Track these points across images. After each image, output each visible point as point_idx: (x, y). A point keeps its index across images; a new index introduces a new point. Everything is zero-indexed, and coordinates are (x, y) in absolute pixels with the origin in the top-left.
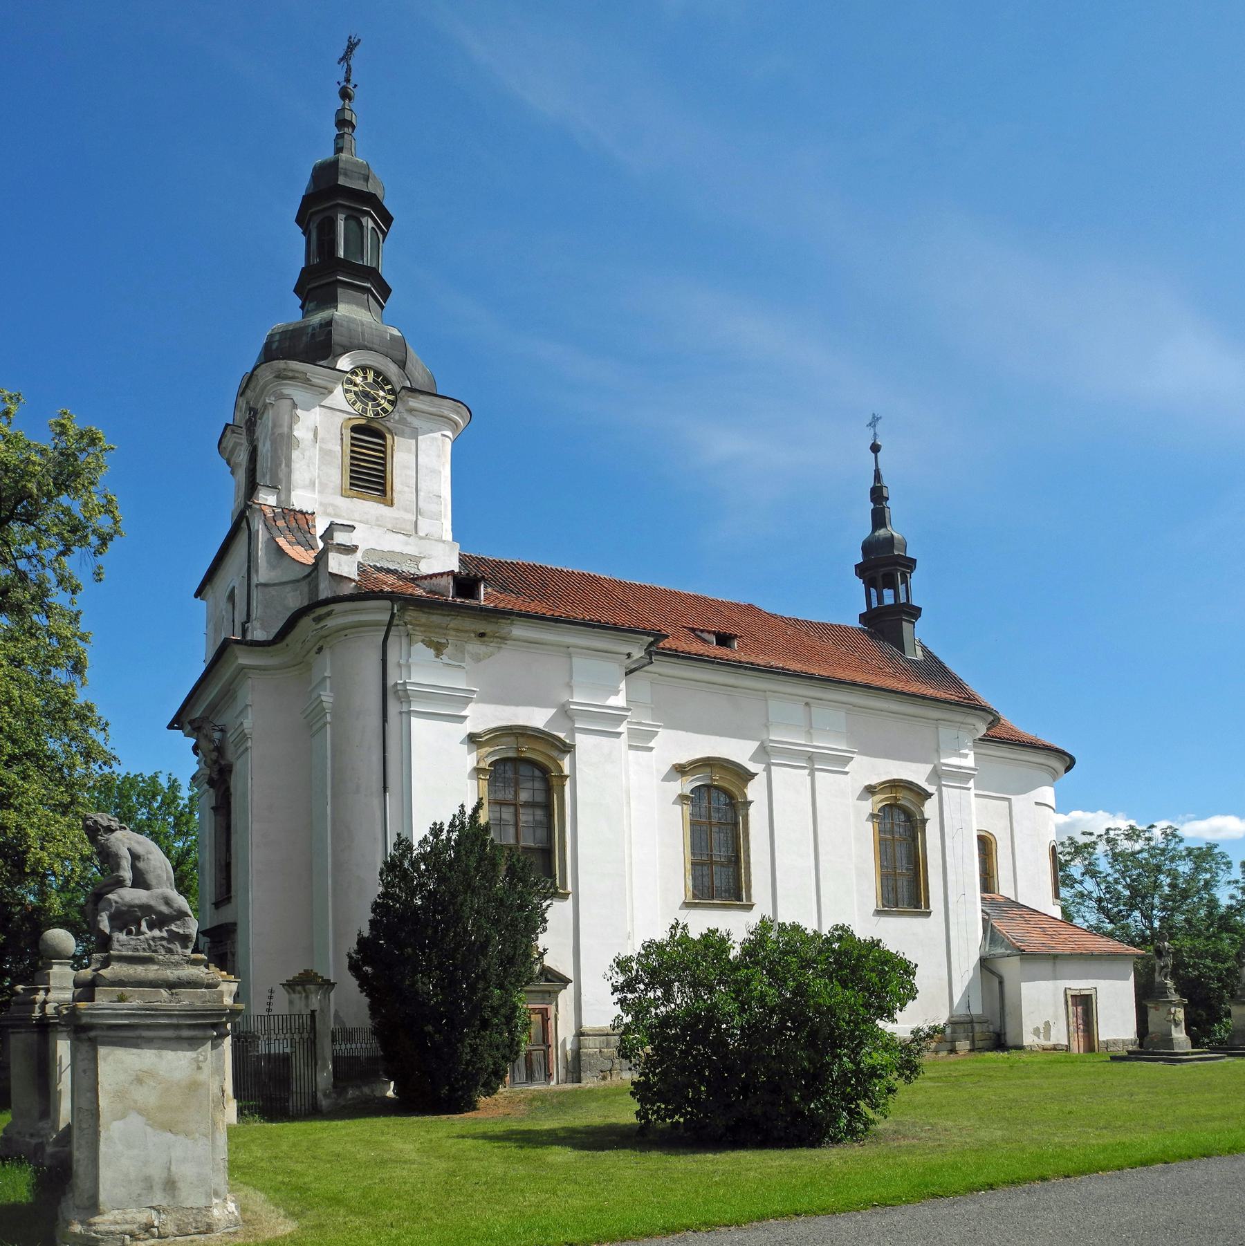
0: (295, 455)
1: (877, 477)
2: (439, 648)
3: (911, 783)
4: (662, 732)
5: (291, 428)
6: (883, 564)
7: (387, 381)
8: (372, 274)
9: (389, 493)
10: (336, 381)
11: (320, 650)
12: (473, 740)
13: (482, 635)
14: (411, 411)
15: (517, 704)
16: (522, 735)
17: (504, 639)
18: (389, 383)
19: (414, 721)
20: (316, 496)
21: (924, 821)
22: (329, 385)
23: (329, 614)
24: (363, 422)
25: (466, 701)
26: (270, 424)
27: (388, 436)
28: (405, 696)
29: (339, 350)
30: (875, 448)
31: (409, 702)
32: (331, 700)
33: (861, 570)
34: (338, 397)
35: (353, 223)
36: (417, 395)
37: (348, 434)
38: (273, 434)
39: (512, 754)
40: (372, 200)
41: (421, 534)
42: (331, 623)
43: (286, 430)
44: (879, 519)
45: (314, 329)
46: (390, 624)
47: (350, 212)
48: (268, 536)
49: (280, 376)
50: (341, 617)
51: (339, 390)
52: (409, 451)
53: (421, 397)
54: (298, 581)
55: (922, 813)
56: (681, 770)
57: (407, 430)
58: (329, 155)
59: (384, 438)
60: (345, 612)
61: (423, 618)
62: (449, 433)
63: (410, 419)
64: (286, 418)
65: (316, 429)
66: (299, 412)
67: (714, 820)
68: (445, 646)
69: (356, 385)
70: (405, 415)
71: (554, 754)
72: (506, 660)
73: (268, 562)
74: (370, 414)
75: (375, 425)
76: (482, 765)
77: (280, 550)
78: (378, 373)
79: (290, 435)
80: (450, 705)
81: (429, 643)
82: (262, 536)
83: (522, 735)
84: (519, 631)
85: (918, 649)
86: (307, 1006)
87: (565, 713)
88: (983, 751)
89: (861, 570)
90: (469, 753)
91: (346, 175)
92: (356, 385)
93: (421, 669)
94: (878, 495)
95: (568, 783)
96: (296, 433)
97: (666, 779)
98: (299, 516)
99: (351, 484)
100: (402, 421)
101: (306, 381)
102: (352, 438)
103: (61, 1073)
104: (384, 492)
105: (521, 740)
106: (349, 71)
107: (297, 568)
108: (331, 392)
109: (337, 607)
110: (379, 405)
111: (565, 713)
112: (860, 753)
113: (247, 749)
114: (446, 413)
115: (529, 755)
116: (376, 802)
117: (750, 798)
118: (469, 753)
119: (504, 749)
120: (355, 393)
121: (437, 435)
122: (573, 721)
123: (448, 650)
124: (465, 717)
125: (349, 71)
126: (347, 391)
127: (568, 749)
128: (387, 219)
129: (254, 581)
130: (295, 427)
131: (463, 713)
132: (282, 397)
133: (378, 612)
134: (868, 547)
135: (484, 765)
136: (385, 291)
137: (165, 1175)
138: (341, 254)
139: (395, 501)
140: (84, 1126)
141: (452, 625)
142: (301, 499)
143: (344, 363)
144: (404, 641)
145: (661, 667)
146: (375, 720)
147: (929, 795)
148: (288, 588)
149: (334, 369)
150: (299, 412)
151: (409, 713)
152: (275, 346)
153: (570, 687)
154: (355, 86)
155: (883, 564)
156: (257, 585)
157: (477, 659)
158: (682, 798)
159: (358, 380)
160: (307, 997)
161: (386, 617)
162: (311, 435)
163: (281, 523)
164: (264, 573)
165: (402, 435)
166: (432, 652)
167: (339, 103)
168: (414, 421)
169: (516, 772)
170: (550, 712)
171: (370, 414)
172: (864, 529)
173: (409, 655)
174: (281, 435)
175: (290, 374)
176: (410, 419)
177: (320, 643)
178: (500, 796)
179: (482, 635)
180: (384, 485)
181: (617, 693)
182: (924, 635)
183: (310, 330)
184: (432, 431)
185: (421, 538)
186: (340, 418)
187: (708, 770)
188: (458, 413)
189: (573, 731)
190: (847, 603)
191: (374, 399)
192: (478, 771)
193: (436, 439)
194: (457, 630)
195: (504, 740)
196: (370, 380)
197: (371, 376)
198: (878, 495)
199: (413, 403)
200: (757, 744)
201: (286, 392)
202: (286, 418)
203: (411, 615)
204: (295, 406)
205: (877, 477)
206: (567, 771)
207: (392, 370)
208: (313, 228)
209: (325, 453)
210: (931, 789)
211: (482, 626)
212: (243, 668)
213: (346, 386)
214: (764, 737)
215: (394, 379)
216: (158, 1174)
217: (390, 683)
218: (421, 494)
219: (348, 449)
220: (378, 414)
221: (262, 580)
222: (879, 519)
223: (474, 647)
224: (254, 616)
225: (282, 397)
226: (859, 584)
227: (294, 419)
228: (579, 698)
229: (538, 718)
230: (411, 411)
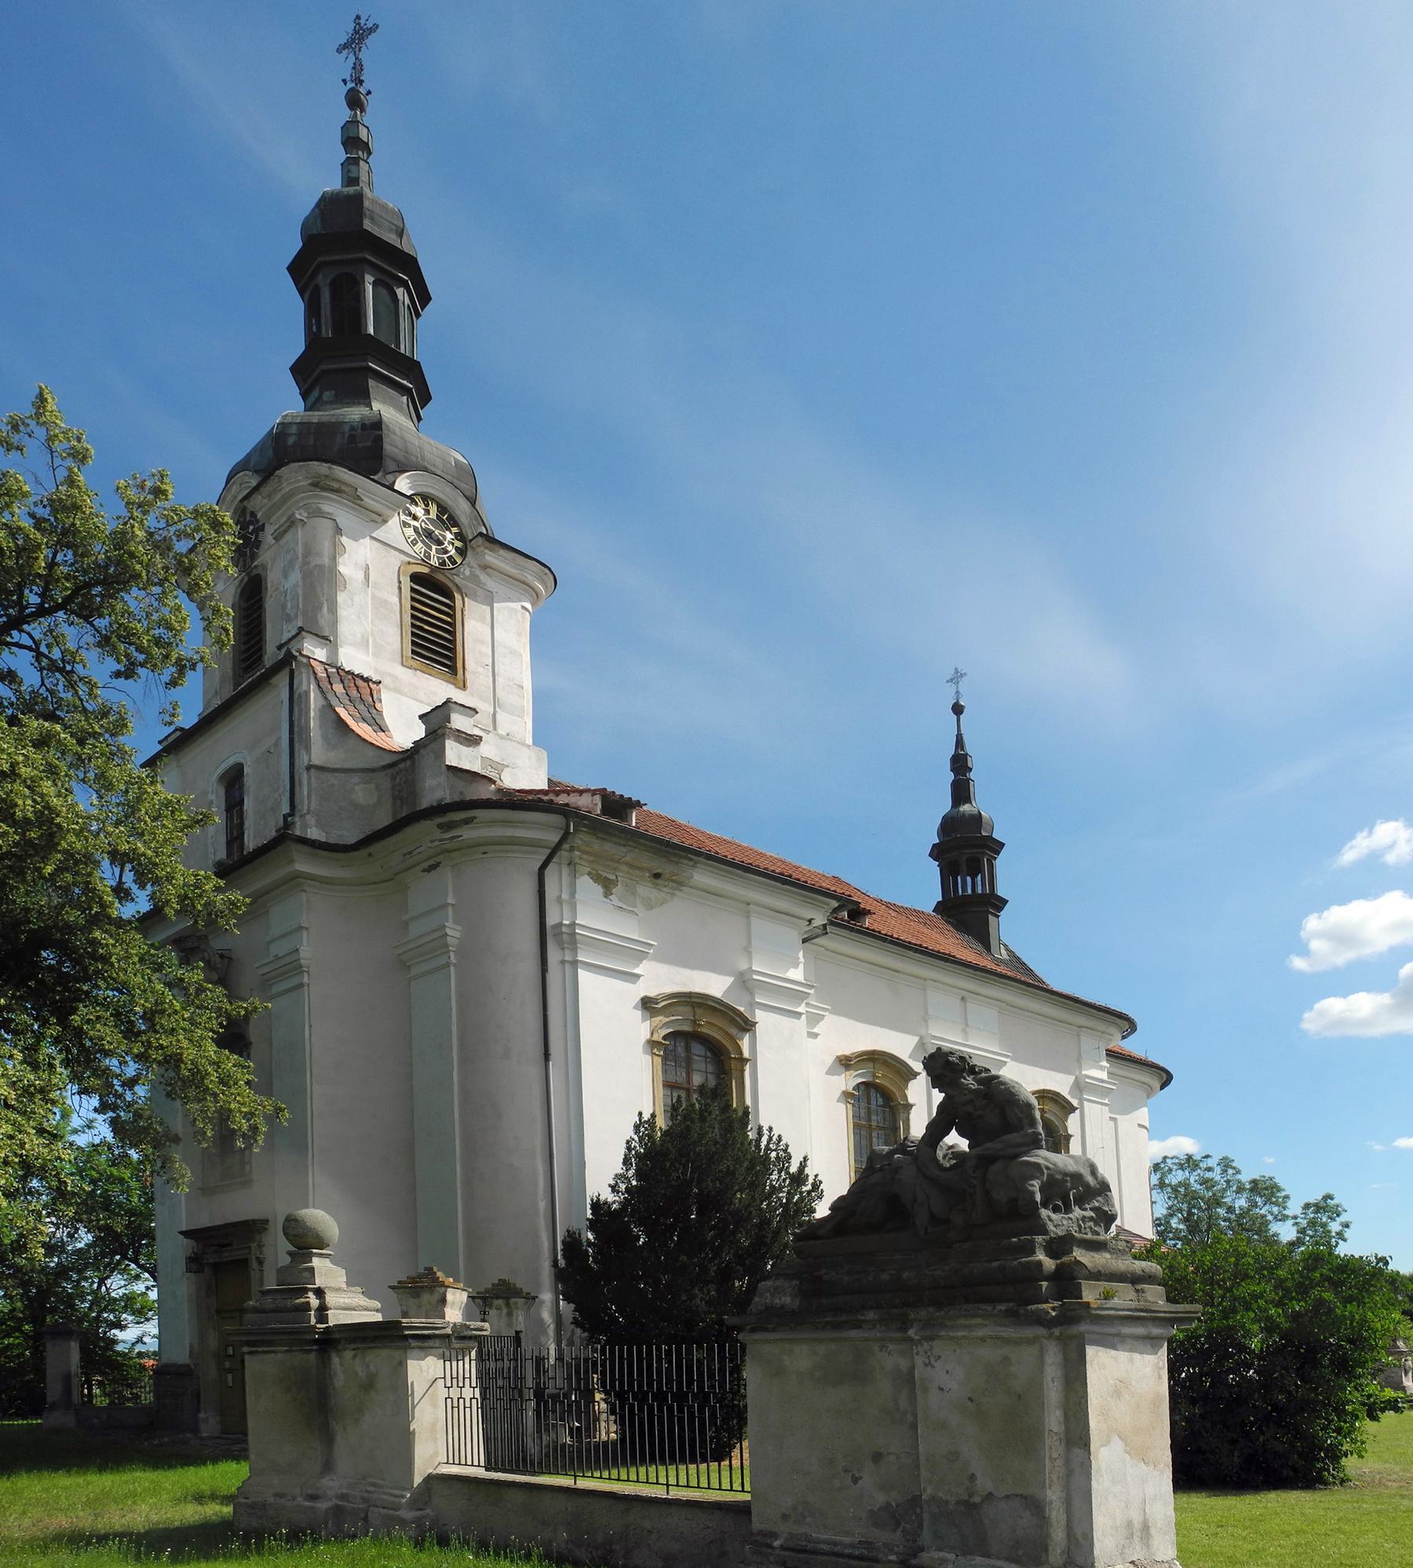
0: (341, 598)
1: (960, 742)
2: (608, 886)
3: (1058, 1094)
4: (830, 1018)
5: (334, 559)
6: (964, 848)
7: (453, 522)
8: (412, 368)
9: (460, 672)
10: (395, 507)
11: (433, 867)
12: (648, 1005)
13: (657, 876)
14: (485, 567)
15: (693, 968)
16: (700, 1005)
17: (680, 884)
18: (456, 524)
19: (583, 975)
20: (370, 659)
21: (1068, 1137)
22: (386, 512)
23: (467, 822)
24: (426, 570)
25: (641, 956)
26: (300, 550)
27: (457, 596)
28: (570, 938)
29: (392, 466)
30: (958, 709)
31: (575, 950)
32: (458, 935)
33: (937, 853)
34: (394, 529)
35: (384, 292)
36: (496, 547)
37: (407, 584)
38: (306, 563)
39: (687, 1028)
40: (410, 265)
41: (502, 731)
42: (468, 834)
43: (326, 561)
44: (961, 791)
45: (352, 428)
46: (555, 850)
47: (382, 277)
48: (323, 702)
49: (319, 484)
50: (485, 827)
51: (394, 522)
52: (483, 621)
53: (502, 552)
54: (373, 770)
55: (1066, 1128)
56: (845, 1063)
57: (480, 592)
58: (333, 183)
59: (452, 598)
60: (493, 823)
61: (596, 845)
62: (528, 606)
63: (483, 577)
64: (327, 544)
65: (367, 570)
66: (344, 539)
67: (874, 1124)
68: (615, 883)
69: (415, 518)
70: (478, 572)
71: (733, 1031)
72: (680, 912)
73: (325, 738)
74: (434, 562)
75: (440, 577)
76: (656, 1038)
77: (342, 724)
78: (442, 509)
79: (333, 570)
80: (622, 958)
81: (597, 878)
82: (314, 699)
83: (700, 1005)
84: (702, 877)
85: (1003, 951)
86: (510, 1325)
87: (744, 982)
88: (1120, 1072)
89: (937, 853)
90: (644, 1020)
91: (372, 219)
92: (415, 518)
93: (591, 911)
94: (960, 764)
95: (747, 1068)
96: (341, 568)
97: (831, 1072)
98: (360, 683)
99: (413, 652)
100: (474, 578)
101: (356, 499)
102: (413, 590)
103: (414, 1407)
104: (452, 669)
105: (699, 1011)
106: (358, 67)
107: (370, 752)
108: (385, 522)
109: (481, 814)
110: (446, 552)
111: (744, 982)
112: (1014, 1059)
113: (301, 985)
114: (530, 579)
115: (705, 1030)
116: (534, 1071)
117: (911, 1100)
118: (644, 1020)
119: (678, 1020)
120: (416, 529)
121: (517, 606)
122: (752, 995)
123: (618, 889)
124: (638, 976)
125: (358, 67)
126: (405, 524)
127: (748, 1026)
128: (425, 297)
129: (303, 759)
130: (340, 560)
131: (636, 971)
132: (319, 514)
133: (543, 830)
134: (949, 825)
135: (658, 1037)
136: (425, 397)
137: (1141, 1519)
138: (371, 331)
139: (468, 684)
140: (1055, 1455)
141: (628, 859)
142: (352, 659)
143: (403, 484)
144: (565, 871)
145: (838, 943)
146: (528, 967)
147: (1073, 1109)
148: (356, 778)
149: (391, 487)
150: (344, 539)
151: (575, 963)
152: (291, 441)
153: (747, 950)
154: (369, 93)
155: (964, 848)
156: (309, 768)
157: (649, 906)
158: (846, 1095)
159: (419, 511)
160: (510, 1314)
161: (554, 838)
162: (360, 575)
163: (338, 688)
164: (318, 751)
165: (474, 598)
166: (599, 889)
167: (346, 114)
168: (490, 583)
169: (688, 1049)
170: (729, 980)
171: (434, 562)
172: (945, 805)
173: (573, 894)
174: (321, 567)
175: (335, 485)
176: (483, 577)
177: (438, 859)
178: (671, 1078)
179: (657, 876)
180: (453, 659)
181: (796, 966)
182: (1012, 930)
183: (347, 429)
184: (510, 600)
185: (502, 737)
186: (396, 560)
187: (871, 1065)
188: (543, 582)
189: (753, 1005)
190: (923, 888)
191: (439, 543)
192: (652, 1044)
193: (512, 610)
194: (631, 866)
195: (680, 1009)
196: (433, 515)
197: (433, 509)
198: (960, 764)
199: (491, 557)
200: (916, 1039)
201: (327, 508)
202: (327, 544)
203: (582, 839)
204: (338, 531)
205: (960, 742)
206: (746, 1054)
207: (461, 508)
208: (323, 282)
209: (380, 603)
210: (1075, 1103)
211: (658, 865)
212: (297, 876)
213: (403, 517)
214: (923, 1033)
215: (464, 520)
216: (1136, 1517)
217: (551, 920)
218: (500, 680)
219: (407, 603)
220: (443, 563)
221: (316, 761)
222: (961, 791)
223: (645, 890)
224: (303, 806)
225: (319, 514)
226: (934, 868)
227: (336, 550)
228: (761, 966)
229: (716, 985)
230: (485, 567)
